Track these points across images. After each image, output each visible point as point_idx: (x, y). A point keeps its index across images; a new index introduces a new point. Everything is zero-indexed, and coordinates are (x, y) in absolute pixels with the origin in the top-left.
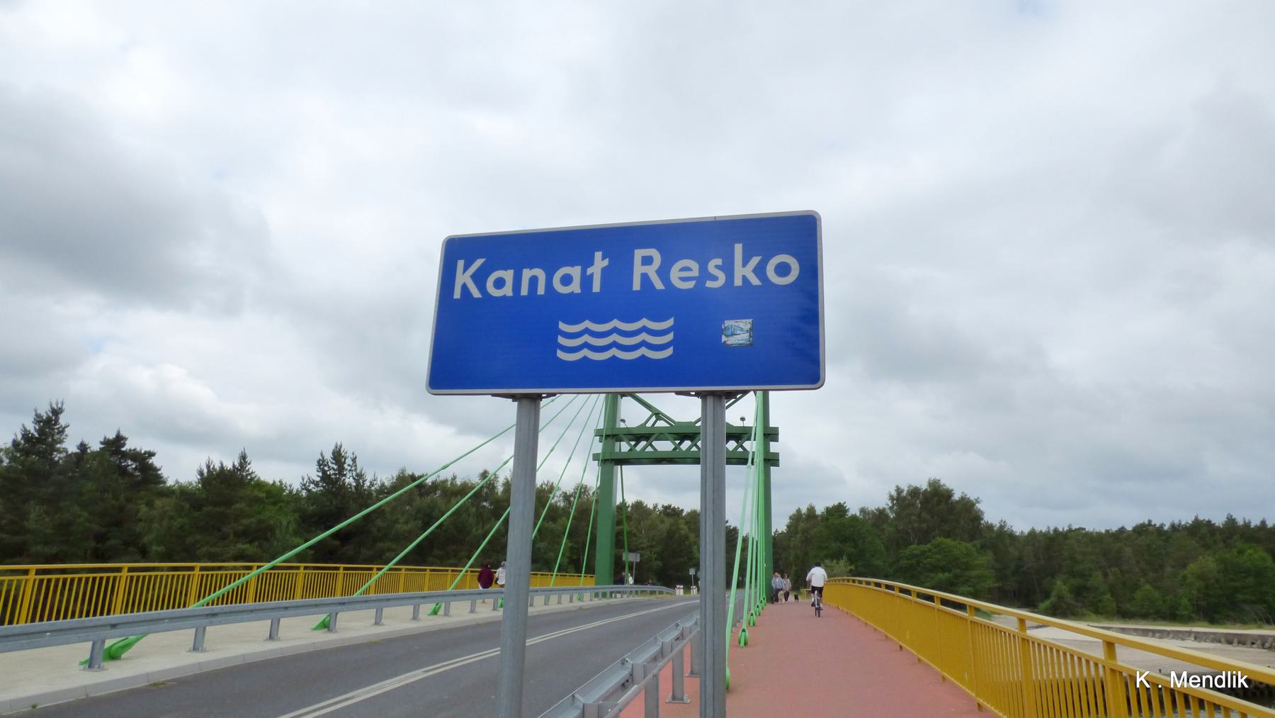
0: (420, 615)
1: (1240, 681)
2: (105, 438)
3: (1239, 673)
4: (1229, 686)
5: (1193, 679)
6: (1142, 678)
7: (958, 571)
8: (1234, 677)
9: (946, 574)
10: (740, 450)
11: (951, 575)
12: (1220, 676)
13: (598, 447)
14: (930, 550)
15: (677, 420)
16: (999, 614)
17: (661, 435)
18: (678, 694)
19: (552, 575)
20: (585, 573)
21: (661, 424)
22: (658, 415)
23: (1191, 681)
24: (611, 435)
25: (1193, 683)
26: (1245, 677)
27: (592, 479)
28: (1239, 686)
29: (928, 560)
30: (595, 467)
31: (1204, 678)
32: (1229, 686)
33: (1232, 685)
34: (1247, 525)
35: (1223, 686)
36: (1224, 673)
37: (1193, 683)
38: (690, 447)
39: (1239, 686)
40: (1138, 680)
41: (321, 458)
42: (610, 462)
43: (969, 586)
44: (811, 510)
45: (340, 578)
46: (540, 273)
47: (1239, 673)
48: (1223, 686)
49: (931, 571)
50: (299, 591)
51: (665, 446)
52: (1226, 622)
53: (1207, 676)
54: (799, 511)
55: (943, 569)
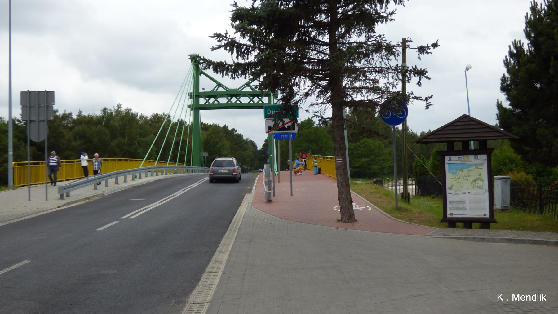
0: (109, 184)
1: (543, 298)
3: (542, 294)
4: (538, 300)
5: (522, 297)
6: (500, 297)
7: (373, 157)
8: (540, 296)
9: (367, 159)
10: (260, 102)
11: (369, 159)
12: (534, 296)
13: (190, 102)
14: (359, 146)
15: (229, 88)
17: (222, 95)
18: (152, 175)
19: (167, 163)
20: (170, 161)
21: (221, 89)
22: (219, 85)
23: (521, 298)
24: (196, 95)
25: (524, 297)
26: (545, 296)
28: (542, 300)
29: (357, 151)
30: (190, 113)
31: (527, 296)
32: (538, 300)
34: (261, 148)
36: (536, 294)
37: (524, 297)
38: (214, 101)
39: (542, 300)
40: (498, 297)
42: (196, 109)
43: (378, 165)
44: (306, 120)
45: (76, 165)
46: (530, 296)
47: (542, 294)
48: (535, 300)
49: (358, 157)
50: (29, 158)
51: (223, 101)
53: (528, 296)
54: (306, 120)
55: (365, 156)
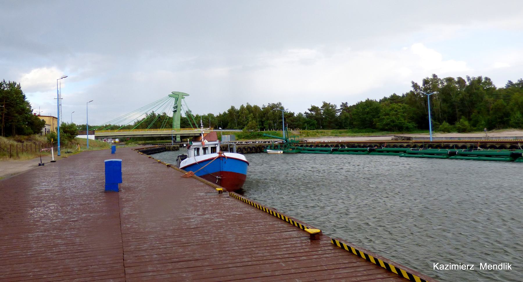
1: (509, 267)
2: (312, 106)
6: (436, 266)
8: (506, 265)
11: (230, 123)
23: (462, 267)
26: (511, 265)
28: (508, 269)
32: (506, 269)
33: (505, 269)
35: (452, 265)
39: (508, 269)
40: (434, 266)
41: (316, 239)
48: (502, 269)
52: (508, 127)
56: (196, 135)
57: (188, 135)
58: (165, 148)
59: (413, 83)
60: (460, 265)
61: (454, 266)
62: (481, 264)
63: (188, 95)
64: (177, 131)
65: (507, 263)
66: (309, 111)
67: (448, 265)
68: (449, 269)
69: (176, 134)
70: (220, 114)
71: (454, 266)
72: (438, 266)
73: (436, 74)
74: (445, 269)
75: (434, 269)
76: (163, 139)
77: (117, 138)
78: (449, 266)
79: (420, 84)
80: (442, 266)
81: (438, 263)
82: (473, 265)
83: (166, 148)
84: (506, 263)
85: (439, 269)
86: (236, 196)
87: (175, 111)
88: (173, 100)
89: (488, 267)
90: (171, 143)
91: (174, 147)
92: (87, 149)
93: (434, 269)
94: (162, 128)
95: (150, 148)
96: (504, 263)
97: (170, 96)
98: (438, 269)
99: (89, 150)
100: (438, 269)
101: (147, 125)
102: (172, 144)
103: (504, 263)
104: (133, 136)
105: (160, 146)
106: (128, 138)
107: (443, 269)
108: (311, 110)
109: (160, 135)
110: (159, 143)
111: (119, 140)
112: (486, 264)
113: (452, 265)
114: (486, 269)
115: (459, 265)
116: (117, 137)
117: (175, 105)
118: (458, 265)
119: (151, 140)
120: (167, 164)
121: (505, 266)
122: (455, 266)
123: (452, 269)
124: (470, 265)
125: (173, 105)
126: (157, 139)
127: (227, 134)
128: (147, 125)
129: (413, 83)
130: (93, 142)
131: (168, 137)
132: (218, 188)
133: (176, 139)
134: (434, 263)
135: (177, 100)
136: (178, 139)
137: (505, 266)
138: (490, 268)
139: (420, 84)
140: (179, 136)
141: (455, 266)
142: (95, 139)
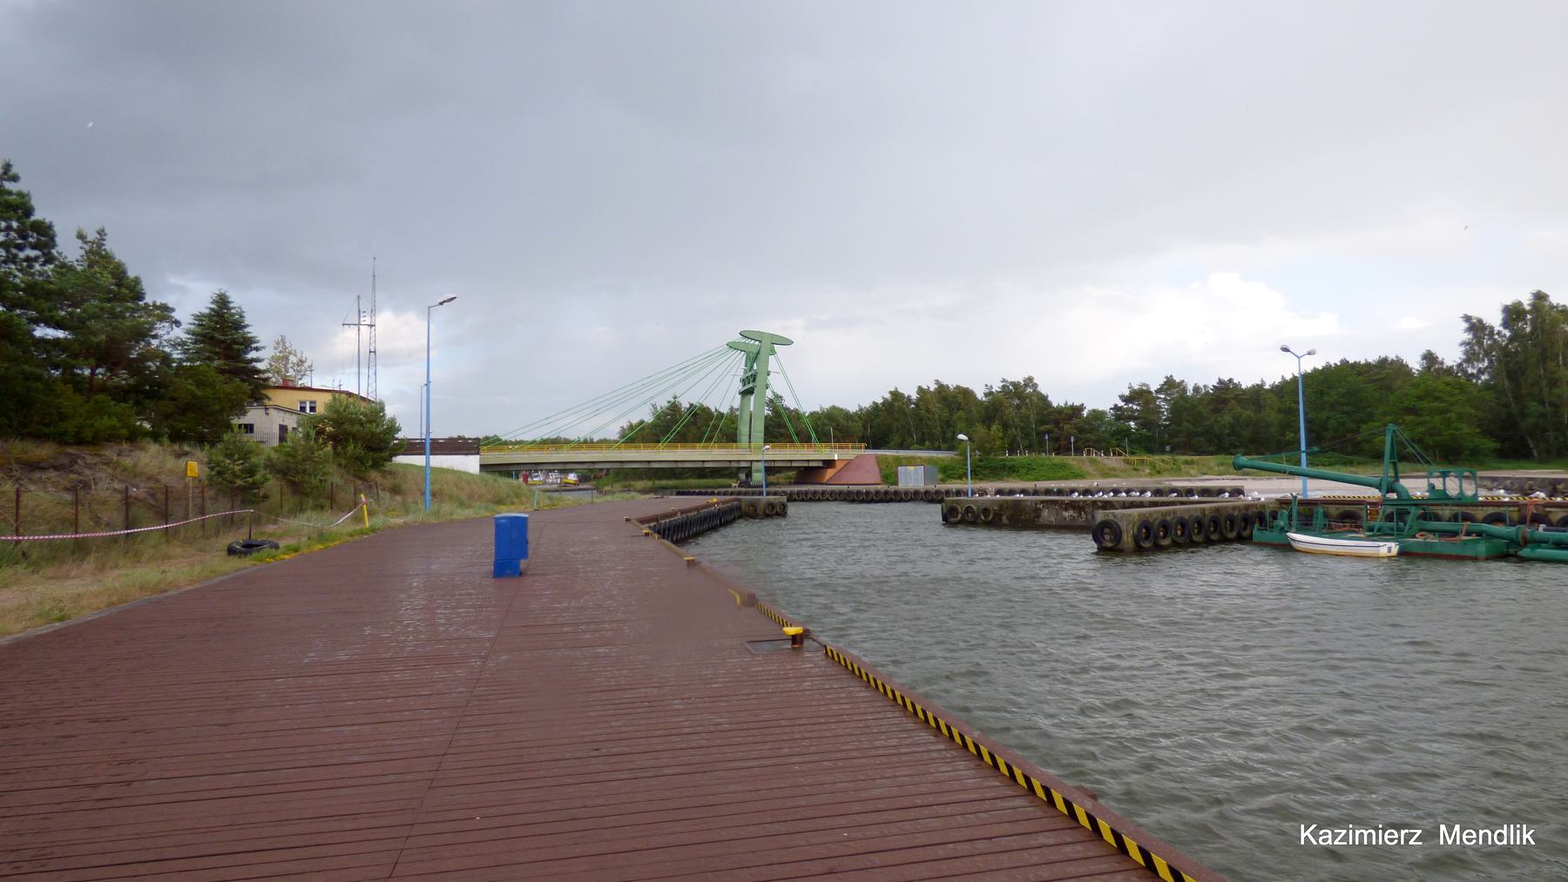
1: (1526, 836)
8: (1518, 832)
16: (1450, 735)
23: (1386, 837)
26: (1532, 831)
27: (737, 403)
28: (1525, 843)
32: (1518, 843)
33: (1515, 840)
39: (1525, 843)
40: (1303, 836)
48: (1505, 842)
53: (1485, 831)
56: (811, 464)
57: (788, 465)
58: (739, 508)
59: (1467, 318)
60: (1380, 831)
61: (1362, 834)
62: (1443, 828)
63: (787, 342)
64: (754, 451)
65: (1522, 826)
66: (1123, 401)
67: (1344, 832)
68: (1345, 843)
69: (751, 461)
70: (861, 409)
71: (1362, 834)
72: (1315, 835)
73: (1545, 290)
74: (1336, 843)
75: (1303, 843)
76: (704, 476)
77: (571, 471)
78: (1347, 835)
79: (1494, 319)
80: (1326, 834)
81: (1314, 826)
82: (1419, 832)
83: (743, 506)
84: (1518, 826)
85: (1318, 842)
86: (831, 651)
87: (747, 393)
88: (740, 358)
89: (1464, 837)
90: (760, 489)
91: (771, 505)
92: (420, 517)
93: (1303, 843)
94: (709, 440)
95: (697, 509)
96: (1512, 826)
97: (732, 346)
98: (1315, 843)
99: (433, 520)
100: (1315, 843)
101: (658, 436)
102: (761, 493)
103: (1512, 826)
104: (619, 466)
105: (723, 503)
106: (601, 470)
107: (1330, 842)
108: (1127, 400)
109: (703, 461)
110: (699, 487)
111: (578, 477)
112: (1457, 828)
113: (1357, 832)
114: (1458, 843)
115: (1377, 829)
116: (568, 467)
117: (749, 374)
118: (1373, 832)
119: (668, 478)
120: (686, 559)
121: (1515, 834)
122: (1366, 833)
123: (1357, 843)
124: (1411, 831)
125: (741, 374)
126: (686, 475)
127: (911, 462)
128: (658, 436)
129: (1467, 318)
130: (469, 483)
131: (719, 471)
132: (791, 626)
133: (749, 475)
134: (1303, 826)
135: (753, 358)
136: (758, 477)
137: (1515, 834)
138: (1469, 840)
139: (1494, 319)
140: (761, 466)
141: (1366, 833)
142: (480, 471)
